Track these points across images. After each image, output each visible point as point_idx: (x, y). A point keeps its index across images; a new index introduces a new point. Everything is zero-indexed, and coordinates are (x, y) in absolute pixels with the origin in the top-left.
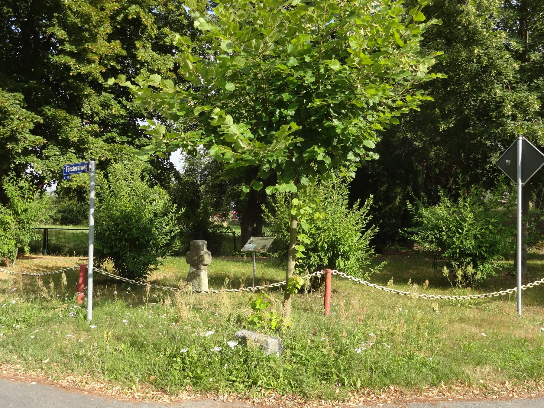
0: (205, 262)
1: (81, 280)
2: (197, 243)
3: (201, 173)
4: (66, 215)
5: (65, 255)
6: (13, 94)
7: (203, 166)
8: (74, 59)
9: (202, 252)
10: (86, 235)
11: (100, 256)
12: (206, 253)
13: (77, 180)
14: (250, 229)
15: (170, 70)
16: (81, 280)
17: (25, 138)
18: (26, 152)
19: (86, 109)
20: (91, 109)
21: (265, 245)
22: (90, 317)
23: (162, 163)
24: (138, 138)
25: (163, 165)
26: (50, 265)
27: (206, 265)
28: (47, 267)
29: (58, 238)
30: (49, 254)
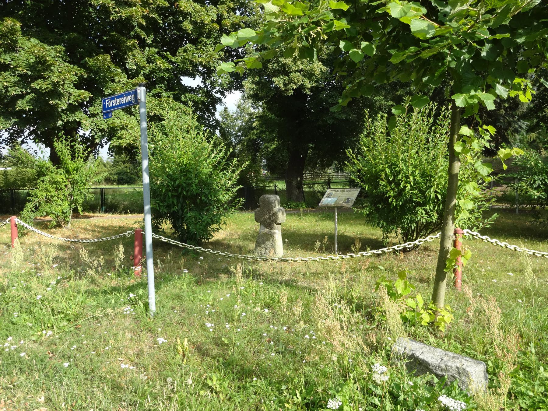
0: (279, 221)
1: (137, 250)
2: (269, 199)
3: (236, 134)
4: (121, 176)
5: (121, 213)
6: (54, 47)
7: (237, 128)
8: (114, 2)
9: (275, 210)
10: (141, 194)
11: (157, 216)
12: (280, 210)
13: (126, 137)
14: (294, 183)
15: (213, 21)
16: (137, 250)
17: (69, 93)
18: (72, 109)
19: (131, 65)
20: (136, 64)
21: (348, 198)
22: (153, 307)
23: (208, 120)
24: (184, 94)
25: (209, 122)
26: (106, 225)
27: (280, 224)
28: (103, 227)
29: (115, 197)
30: (106, 212)
